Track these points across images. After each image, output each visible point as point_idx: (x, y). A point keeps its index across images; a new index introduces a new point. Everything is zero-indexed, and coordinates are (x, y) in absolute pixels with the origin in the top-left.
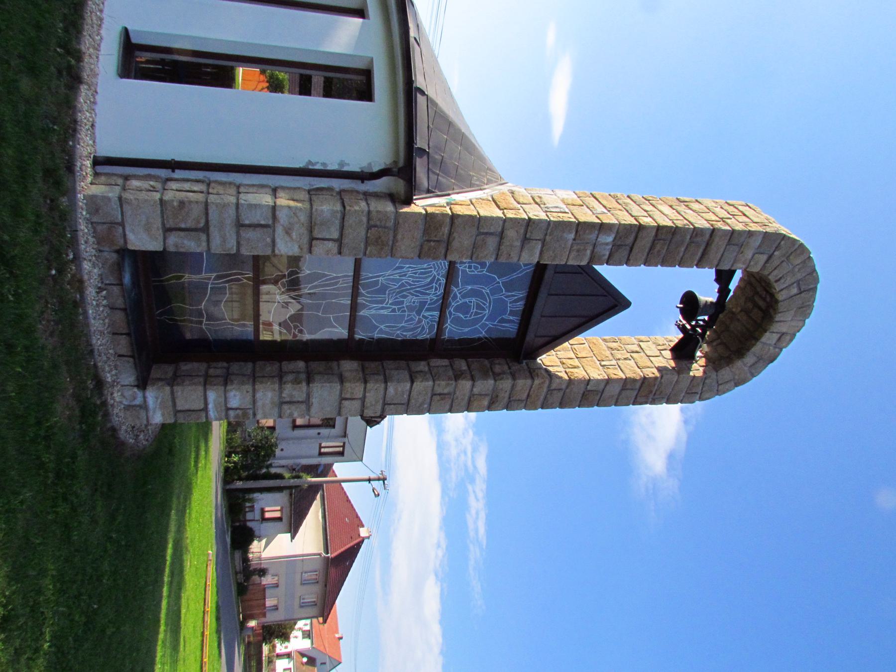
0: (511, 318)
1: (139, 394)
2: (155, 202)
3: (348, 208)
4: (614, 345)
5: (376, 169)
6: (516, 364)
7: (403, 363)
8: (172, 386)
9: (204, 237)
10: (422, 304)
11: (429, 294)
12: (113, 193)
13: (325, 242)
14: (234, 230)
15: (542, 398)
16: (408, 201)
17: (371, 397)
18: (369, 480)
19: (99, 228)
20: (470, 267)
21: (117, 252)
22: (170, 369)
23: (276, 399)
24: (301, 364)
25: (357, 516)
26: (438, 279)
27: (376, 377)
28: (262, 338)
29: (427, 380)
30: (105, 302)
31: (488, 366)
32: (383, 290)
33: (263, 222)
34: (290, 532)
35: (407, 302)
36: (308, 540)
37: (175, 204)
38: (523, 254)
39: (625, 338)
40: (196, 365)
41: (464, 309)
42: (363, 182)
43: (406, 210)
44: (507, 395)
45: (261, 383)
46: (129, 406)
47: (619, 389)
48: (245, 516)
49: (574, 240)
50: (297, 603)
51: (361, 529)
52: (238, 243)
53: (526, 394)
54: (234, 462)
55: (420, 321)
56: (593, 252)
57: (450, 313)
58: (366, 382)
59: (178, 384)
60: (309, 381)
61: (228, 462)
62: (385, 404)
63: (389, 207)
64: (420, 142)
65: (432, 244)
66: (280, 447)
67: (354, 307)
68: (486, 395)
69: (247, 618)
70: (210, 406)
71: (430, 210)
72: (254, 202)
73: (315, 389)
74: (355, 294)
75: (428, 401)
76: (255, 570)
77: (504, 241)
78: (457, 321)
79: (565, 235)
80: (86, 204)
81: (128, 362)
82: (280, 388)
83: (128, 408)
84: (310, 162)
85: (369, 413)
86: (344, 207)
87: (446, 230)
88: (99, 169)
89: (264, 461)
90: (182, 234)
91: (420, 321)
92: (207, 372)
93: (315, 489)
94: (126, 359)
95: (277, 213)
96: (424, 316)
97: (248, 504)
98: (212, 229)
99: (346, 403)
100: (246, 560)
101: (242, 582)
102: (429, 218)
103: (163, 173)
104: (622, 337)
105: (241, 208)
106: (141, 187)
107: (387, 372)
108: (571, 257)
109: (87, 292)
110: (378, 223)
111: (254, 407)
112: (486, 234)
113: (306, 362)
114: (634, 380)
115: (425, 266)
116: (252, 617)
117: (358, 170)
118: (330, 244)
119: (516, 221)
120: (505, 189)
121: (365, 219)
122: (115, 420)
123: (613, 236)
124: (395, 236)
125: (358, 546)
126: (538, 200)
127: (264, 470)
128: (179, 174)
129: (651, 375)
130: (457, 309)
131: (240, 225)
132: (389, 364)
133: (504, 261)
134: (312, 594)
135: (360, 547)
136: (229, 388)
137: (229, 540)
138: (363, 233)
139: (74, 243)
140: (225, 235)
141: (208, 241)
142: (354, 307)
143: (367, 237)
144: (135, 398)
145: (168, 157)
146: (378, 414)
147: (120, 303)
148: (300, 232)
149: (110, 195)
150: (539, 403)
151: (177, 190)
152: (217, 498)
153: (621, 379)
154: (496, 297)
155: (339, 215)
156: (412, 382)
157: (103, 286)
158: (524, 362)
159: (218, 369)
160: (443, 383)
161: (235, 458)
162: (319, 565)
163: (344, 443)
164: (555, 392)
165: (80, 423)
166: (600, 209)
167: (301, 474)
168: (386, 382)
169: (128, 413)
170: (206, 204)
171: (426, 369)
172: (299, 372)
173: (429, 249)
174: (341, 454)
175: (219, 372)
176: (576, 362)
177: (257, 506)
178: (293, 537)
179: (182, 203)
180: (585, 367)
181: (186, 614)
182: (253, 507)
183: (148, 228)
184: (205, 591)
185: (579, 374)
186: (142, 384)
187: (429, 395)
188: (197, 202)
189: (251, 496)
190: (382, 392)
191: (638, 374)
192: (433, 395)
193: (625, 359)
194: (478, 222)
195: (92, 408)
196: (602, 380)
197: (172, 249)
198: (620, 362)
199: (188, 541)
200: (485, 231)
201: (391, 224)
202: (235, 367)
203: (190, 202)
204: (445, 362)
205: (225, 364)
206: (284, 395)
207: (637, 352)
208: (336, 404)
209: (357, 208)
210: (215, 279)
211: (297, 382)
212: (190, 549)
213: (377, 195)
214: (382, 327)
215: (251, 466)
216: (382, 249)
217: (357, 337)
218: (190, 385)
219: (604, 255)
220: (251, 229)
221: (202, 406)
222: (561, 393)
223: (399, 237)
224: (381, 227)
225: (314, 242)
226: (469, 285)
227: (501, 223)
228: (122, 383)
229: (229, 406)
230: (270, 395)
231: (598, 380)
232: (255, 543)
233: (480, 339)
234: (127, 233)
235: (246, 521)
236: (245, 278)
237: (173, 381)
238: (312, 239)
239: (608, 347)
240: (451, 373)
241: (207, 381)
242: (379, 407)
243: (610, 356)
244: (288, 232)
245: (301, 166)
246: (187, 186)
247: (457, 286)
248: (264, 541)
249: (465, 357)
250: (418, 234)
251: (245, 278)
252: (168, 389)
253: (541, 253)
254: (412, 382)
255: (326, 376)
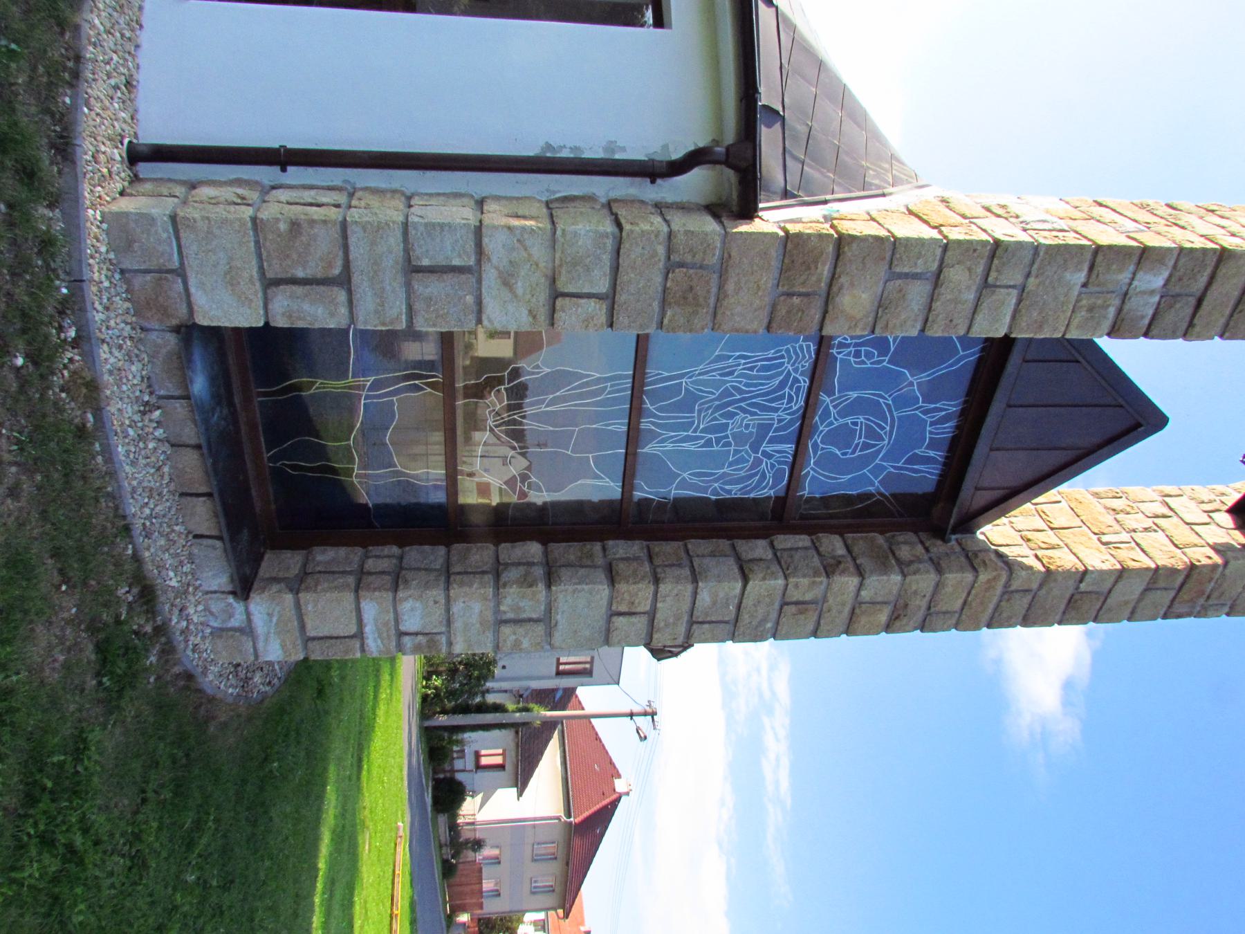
0: (932, 453)
1: (239, 607)
2: (243, 224)
3: (627, 227)
4: (1116, 504)
5: (677, 154)
6: (939, 542)
7: (724, 544)
8: (296, 592)
9: (342, 296)
10: (764, 428)
11: (776, 410)
12: (159, 208)
13: (583, 301)
14: (400, 279)
15: (991, 606)
16: (748, 211)
17: (665, 610)
18: (631, 715)
19: (138, 281)
20: (857, 354)
21: (177, 330)
22: (292, 561)
23: (489, 615)
24: (534, 549)
25: (611, 763)
26: (796, 380)
27: (677, 572)
28: (462, 500)
29: (773, 576)
30: (159, 433)
31: (885, 546)
32: (688, 403)
33: (456, 262)
34: (516, 786)
35: (734, 426)
36: (543, 797)
37: (283, 226)
38: (979, 318)
39: (1135, 491)
40: (342, 551)
41: (842, 437)
42: (653, 182)
43: (744, 228)
44: (924, 603)
45: (462, 584)
46: (222, 629)
47: (1141, 589)
48: (452, 764)
49: (1084, 285)
50: (526, 888)
51: (617, 782)
52: (410, 308)
53: (960, 602)
54: (436, 688)
55: (758, 462)
56: (1120, 311)
57: (815, 446)
58: (657, 581)
59: (307, 589)
60: (550, 579)
61: (427, 687)
62: (692, 623)
63: (709, 225)
64: (767, 96)
65: (796, 300)
66: (500, 664)
67: (633, 437)
68: (886, 603)
69: (456, 910)
70: (368, 629)
71: (793, 228)
72: (439, 219)
73: (561, 596)
74: (635, 411)
75: (774, 615)
76: (467, 842)
77: (942, 290)
78: (828, 462)
79: (1068, 275)
80: (108, 232)
81: (214, 548)
82: (497, 594)
83: (218, 633)
84: (548, 146)
85: (660, 640)
86: (619, 225)
87: (825, 270)
88: (144, 168)
89: (479, 685)
90: (299, 290)
91: (758, 462)
92: (362, 566)
93: (550, 726)
94: (210, 542)
95: (485, 240)
96: (765, 454)
97: (455, 748)
98: (356, 279)
99: (619, 621)
100: (453, 827)
101: (449, 859)
102: (791, 243)
103: (265, 174)
104: (1126, 489)
105: (412, 232)
106: (218, 196)
107: (696, 562)
108: (1075, 322)
109: (112, 409)
110: (688, 258)
111: (449, 632)
112: (906, 276)
113: (544, 543)
114: (1173, 571)
115: (771, 353)
116: (463, 909)
117: (640, 156)
118: (592, 306)
119: (968, 247)
120: (930, 194)
121: (661, 250)
122: (189, 658)
123: (1166, 274)
124: (721, 287)
125: (614, 804)
126: (1001, 212)
127: (478, 699)
128: (295, 174)
129: (1205, 561)
130: (831, 437)
131: (412, 269)
132: (698, 546)
133: (939, 334)
134: (548, 874)
135: (616, 807)
136: (400, 594)
137: (429, 800)
138: (658, 279)
139: (74, 305)
140: (383, 289)
141: (350, 302)
142: (633, 437)
143: (665, 289)
144: (231, 616)
145: (271, 141)
146: (680, 641)
147: (190, 433)
148: (531, 284)
149: (154, 211)
150: (986, 617)
151: (288, 203)
152: (410, 743)
153: (1148, 569)
154: (907, 412)
155: (609, 243)
156: (746, 580)
157: (153, 400)
158: (953, 537)
159: (383, 558)
160: (805, 581)
161: (437, 682)
162: (558, 835)
163: (592, 658)
164: (1017, 596)
165: (98, 674)
166: (1131, 226)
167: (531, 705)
168: (695, 580)
169: (220, 644)
170: (344, 225)
171: (770, 555)
172: (530, 564)
173: (788, 312)
174: (587, 673)
175: (384, 564)
176: (1050, 537)
177: (469, 751)
178: (520, 794)
179: (295, 225)
180: (1072, 546)
181: (362, 927)
182: (463, 751)
183: (231, 278)
184: (393, 883)
185: (1064, 560)
186: (244, 588)
187: (777, 606)
188: (325, 222)
189: (460, 736)
190: (688, 599)
191: (1178, 560)
192: (784, 604)
193: (1146, 530)
194: (890, 250)
195: (127, 645)
196: (1110, 572)
197: (280, 322)
198: (1138, 537)
199: (367, 812)
200: (906, 270)
201: (713, 260)
202: (414, 554)
203: (312, 222)
204: (803, 540)
205: (395, 550)
206: (502, 608)
207: (1164, 516)
208: (602, 623)
209: (647, 227)
210: (370, 389)
211: (527, 582)
212: (370, 824)
213: (683, 207)
214: (685, 475)
215: (457, 698)
216: (695, 313)
217: (638, 494)
218: (330, 589)
219: (1143, 317)
220: (433, 277)
221: (353, 629)
222: (1029, 597)
223: (730, 287)
224: (693, 266)
225: (559, 302)
226: (854, 389)
227: (939, 251)
228: (205, 588)
229: (402, 628)
230: (477, 607)
231: (1102, 572)
232: (469, 799)
233: (868, 496)
234: (193, 290)
235: (453, 771)
236: (428, 384)
237: (297, 584)
238: (556, 295)
239: (1106, 508)
240: (816, 561)
241: (361, 582)
242: (682, 629)
243: (1114, 523)
244: (507, 282)
245: (531, 154)
246: (308, 196)
247: (830, 393)
248: (479, 798)
249: (840, 531)
250: (768, 280)
251: (428, 384)
252: (289, 597)
253: (1014, 317)
254: (746, 580)
255: (582, 572)
